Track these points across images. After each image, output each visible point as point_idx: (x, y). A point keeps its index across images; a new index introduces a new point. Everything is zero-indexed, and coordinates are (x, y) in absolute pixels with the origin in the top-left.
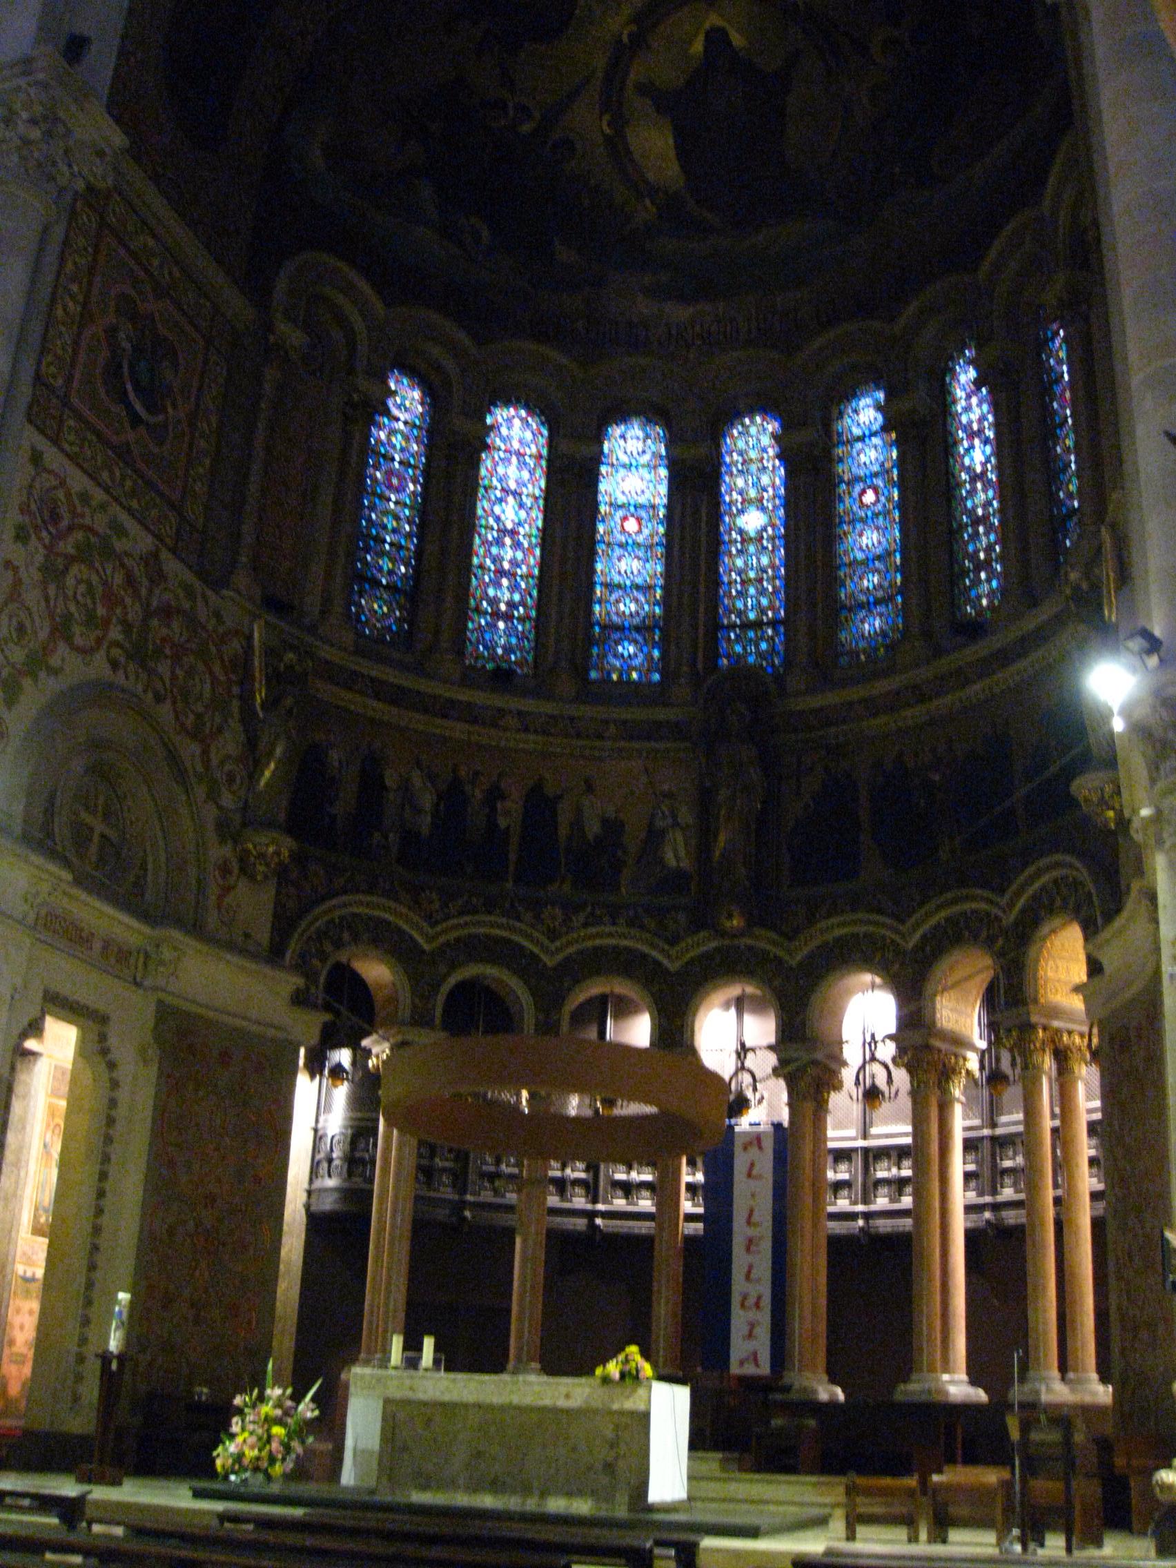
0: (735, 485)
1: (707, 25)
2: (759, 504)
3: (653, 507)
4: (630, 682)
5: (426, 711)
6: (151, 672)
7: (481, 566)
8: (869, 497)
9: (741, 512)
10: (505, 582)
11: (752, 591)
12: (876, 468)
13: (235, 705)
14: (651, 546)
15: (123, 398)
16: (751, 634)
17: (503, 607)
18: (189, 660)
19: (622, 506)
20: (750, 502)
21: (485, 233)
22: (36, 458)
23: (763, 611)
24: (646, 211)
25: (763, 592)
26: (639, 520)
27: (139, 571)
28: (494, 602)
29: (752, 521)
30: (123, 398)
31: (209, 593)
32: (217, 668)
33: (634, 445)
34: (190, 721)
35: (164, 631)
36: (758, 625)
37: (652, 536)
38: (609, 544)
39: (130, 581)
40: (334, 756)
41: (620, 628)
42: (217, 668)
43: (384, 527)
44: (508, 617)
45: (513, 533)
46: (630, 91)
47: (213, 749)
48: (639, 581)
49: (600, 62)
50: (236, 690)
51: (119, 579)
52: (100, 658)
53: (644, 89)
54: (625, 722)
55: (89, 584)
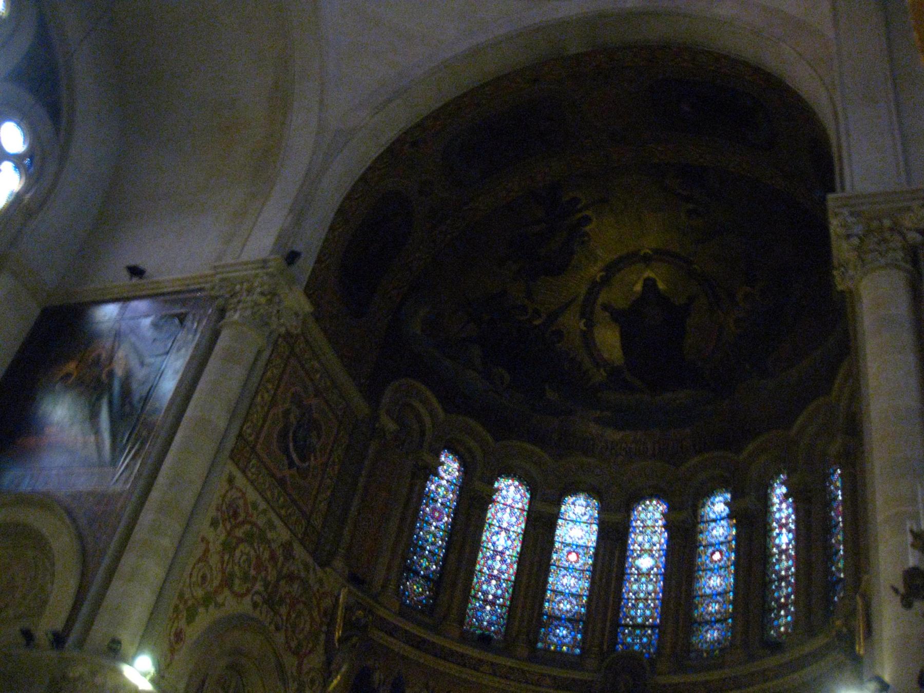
0: (637, 540)
1: (645, 276)
2: (650, 553)
3: (587, 547)
4: (561, 653)
5: (435, 655)
6: (277, 613)
7: (480, 571)
8: (717, 556)
9: (639, 556)
10: (494, 582)
11: (641, 605)
12: (722, 539)
13: (323, 637)
14: (583, 571)
15: (286, 451)
16: (638, 632)
17: (490, 597)
18: (300, 606)
19: (568, 545)
20: (645, 551)
21: (507, 377)
22: (231, 480)
23: (647, 619)
24: (600, 376)
25: (647, 607)
26: (578, 554)
27: (279, 552)
28: (485, 593)
29: (645, 563)
30: (286, 451)
31: (317, 568)
32: (315, 614)
33: (579, 510)
34: (293, 644)
35: (287, 589)
36: (643, 626)
37: (584, 564)
38: (558, 567)
39: (273, 557)
40: (377, 676)
41: (559, 619)
42: (315, 614)
43: (427, 541)
44: (493, 604)
45: (502, 553)
46: (598, 308)
47: (305, 661)
48: (574, 590)
49: (583, 290)
50: (324, 628)
51: (266, 555)
52: (248, 599)
53: (605, 307)
54: (555, 678)
55: (248, 554)
